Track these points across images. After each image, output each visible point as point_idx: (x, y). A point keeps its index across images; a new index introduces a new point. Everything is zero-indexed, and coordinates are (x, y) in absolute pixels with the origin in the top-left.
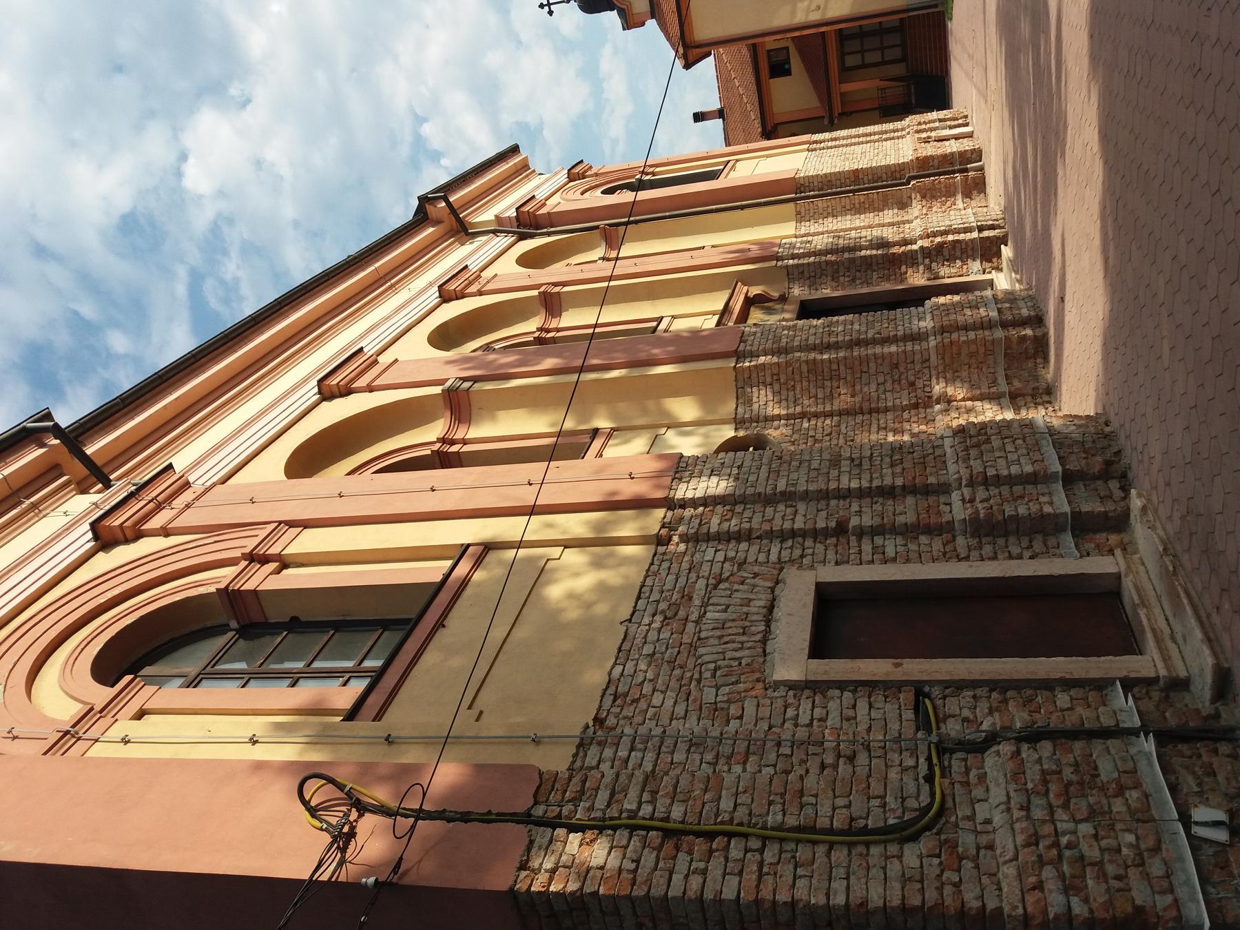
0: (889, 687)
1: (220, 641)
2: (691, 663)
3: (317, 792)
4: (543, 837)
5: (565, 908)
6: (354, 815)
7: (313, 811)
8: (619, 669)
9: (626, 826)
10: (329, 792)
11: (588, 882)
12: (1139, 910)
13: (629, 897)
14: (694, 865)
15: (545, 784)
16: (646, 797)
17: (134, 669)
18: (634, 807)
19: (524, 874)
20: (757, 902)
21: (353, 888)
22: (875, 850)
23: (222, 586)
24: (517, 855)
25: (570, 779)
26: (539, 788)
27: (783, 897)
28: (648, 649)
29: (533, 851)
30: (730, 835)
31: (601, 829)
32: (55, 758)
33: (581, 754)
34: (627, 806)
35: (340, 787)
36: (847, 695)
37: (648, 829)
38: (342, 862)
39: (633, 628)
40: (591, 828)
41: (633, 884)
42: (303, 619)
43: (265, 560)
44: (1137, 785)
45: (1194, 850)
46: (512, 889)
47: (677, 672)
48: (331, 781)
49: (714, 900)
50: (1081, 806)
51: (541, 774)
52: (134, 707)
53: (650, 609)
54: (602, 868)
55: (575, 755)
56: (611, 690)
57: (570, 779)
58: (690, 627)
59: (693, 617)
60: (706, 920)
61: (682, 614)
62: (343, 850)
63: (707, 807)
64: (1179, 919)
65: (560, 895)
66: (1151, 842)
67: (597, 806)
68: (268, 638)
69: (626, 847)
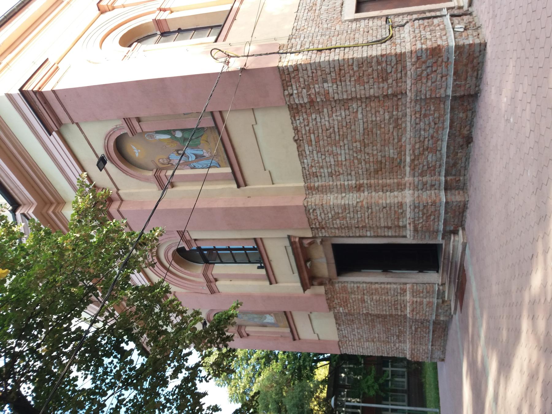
0: (378, 17)
1: (155, 38)
2: (319, 19)
3: (216, 54)
7: (216, 59)
8: (296, 24)
12: (439, 46)
13: (310, 64)
16: (311, 44)
20: (344, 59)
21: (234, 73)
22: (374, 46)
27: (350, 57)
28: (305, 18)
30: (335, 48)
31: (300, 53)
34: (306, 47)
36: (367, 21)
38: (228, 67)
39: (298, 14)
42: (182, 29)
43: (165, 10)
44: (443, 24)
45: (454, 34)
47: (315, 22)
48: (220, 50)
50: (428, 29)
53: (303, 9)
56: (295, 28)
58: (317, 11)
59: (318, 8)
61: (314, 8)
64: (448, 46)
66: (444, 33)
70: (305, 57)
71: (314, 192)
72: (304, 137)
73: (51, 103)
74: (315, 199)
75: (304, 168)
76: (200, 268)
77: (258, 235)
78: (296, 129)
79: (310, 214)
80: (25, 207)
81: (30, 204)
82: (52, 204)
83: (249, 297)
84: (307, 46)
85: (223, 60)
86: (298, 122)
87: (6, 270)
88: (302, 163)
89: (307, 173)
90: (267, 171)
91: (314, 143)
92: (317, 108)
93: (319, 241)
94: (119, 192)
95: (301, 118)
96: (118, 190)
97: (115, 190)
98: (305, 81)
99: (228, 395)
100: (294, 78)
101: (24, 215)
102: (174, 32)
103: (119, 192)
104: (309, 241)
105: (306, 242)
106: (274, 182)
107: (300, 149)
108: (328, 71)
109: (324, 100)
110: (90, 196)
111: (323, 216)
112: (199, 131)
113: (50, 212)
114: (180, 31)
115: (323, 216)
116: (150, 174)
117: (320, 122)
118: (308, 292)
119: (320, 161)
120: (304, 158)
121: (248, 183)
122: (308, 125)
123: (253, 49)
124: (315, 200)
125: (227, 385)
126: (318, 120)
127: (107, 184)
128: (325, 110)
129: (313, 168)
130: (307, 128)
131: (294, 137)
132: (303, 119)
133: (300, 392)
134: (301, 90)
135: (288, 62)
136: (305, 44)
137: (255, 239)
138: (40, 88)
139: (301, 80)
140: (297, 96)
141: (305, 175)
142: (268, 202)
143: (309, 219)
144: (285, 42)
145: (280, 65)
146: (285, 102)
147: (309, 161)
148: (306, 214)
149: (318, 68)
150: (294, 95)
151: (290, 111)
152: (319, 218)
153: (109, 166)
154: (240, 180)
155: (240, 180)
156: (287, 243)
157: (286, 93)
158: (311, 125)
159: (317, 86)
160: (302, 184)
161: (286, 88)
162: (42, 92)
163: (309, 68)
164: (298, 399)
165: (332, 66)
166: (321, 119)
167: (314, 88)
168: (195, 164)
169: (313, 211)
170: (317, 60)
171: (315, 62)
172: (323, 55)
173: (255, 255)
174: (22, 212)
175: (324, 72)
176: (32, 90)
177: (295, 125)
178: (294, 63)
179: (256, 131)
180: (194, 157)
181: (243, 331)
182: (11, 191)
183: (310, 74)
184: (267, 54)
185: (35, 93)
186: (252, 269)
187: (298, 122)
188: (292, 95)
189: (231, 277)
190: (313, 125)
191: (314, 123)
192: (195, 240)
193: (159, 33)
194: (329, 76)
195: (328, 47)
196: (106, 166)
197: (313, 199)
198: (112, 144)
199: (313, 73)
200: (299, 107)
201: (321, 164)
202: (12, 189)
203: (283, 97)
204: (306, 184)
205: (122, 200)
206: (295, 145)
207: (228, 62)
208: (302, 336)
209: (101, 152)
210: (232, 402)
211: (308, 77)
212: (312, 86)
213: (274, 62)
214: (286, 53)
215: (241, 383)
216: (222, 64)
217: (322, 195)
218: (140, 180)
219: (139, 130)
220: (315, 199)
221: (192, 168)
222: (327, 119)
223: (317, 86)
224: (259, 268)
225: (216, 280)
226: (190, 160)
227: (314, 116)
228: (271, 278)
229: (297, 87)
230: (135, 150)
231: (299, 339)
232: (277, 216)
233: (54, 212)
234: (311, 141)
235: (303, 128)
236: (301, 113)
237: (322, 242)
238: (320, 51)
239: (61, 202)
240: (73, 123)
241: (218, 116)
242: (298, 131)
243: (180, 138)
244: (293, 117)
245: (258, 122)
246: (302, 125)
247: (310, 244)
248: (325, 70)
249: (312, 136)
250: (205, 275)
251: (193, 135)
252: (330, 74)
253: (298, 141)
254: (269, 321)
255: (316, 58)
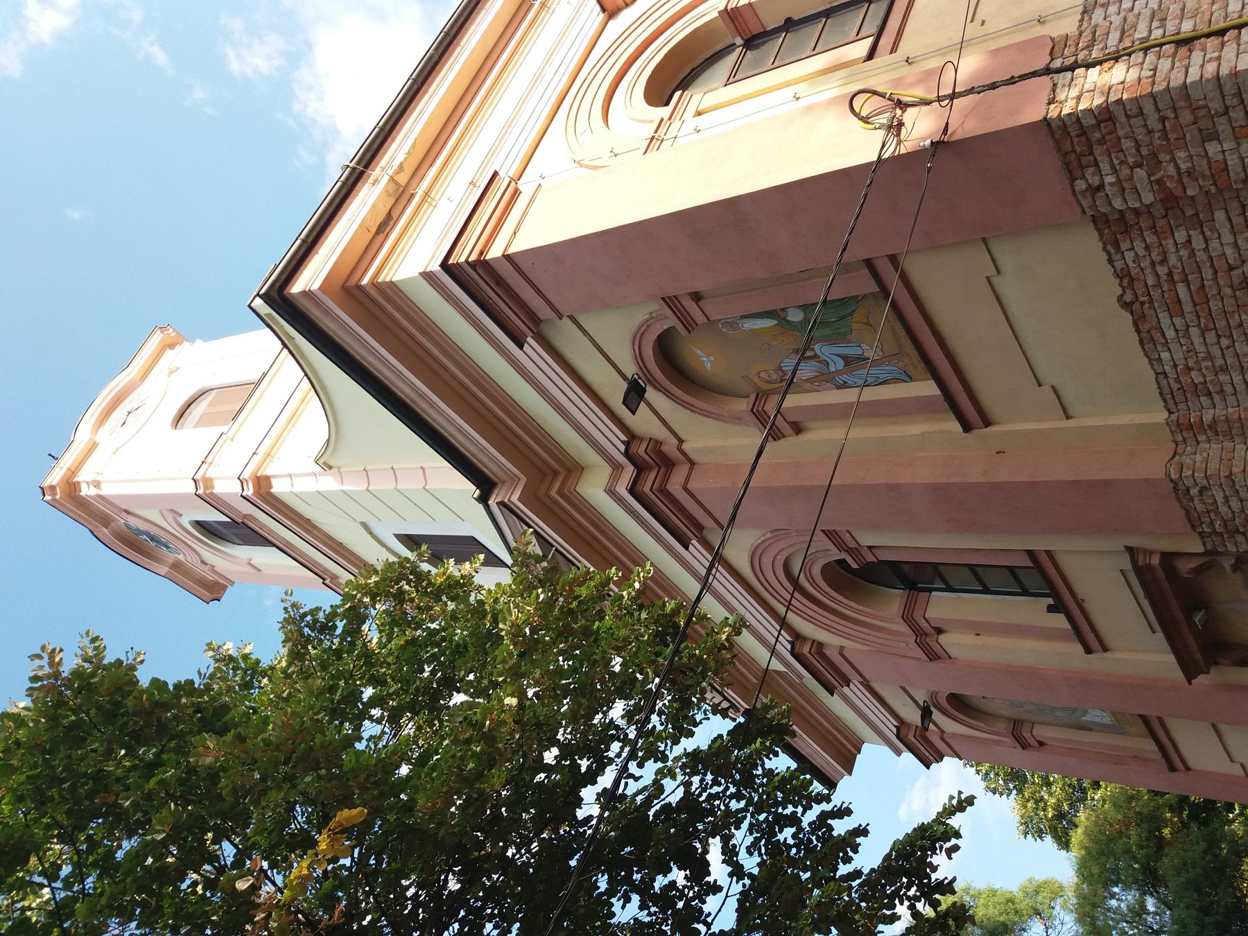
1: (731, 59)
3: (866, 105)
4: (1064, 78)
5: (1094, 122)
6: (899, 112)
7: (866, 120)
9: (1140, 50)
10: (876, 102)
11: (1112, 94)
13: (1152, 96)
14: (1208, 56)
15: (1055, 46)
16: (1155, 24)
17: (684, 84)
18: (1145, 34)
19: (1052, 106)
23: (722, 7)
24: (1045, 96)
25: (1080, 34)
26: (1053, 48)
29: (1058, 90)
31: (1117, 59)
32: (652, 154)
33: (1086, 18)
34: (1137, 36)
35: (882, 95)
37: (1161, 45)
38: (899, 143)
40: (1106, 61)
41: (1154, 83)
42: (796, 18)
46: (1045, 119)
48: (875, 93)
49: (1230, 74)
51: (1052, 40)
52: (691, 110)
54: (1123, 83)
55: (1081, 20)
57: (1080, 34)
60: (1223, 96)
62: (898, 135)
63: (1215, 15)
65: (1089, 111)
67: (1109, 44)
68: (770, 44)
69: (1142, 63)
70: (1133, 74)
71: (1201, 438)
72: (1155, 294)
73: (509, 281)
74: (1207, 457)
75: (1160, 375)
76: (893, 601)
77: (1039, 544)
78: (1123, 275)
79: (1192, 499)
80: (505, 488)
81: (514, 480)
82: (556, 474)
83: (1030, 675)
84: (1141, 32)
85: (884, 119)
86: (1129, 256)
87: (359, 809)
88: (1154, 361)
89: (1175, 386)
90: (1047, 388)
91: (1188, 307)
92: (1190, 212)
93: (1227, 563)
94: (684, 446)
95: (1139, 247)
96: (681, 441)
97: (675, 441)
98: (1138, 146)
99: (1018, 819)
100: (1101, 142)
101: (502, 504)
102: (777, 31)
103: (684, 446)
104: (1194, 563)
105: (1184, 567)
106: (1071, 413)
107: (1144, 327)
108: (1216, 106)
109: (1213, 189)
110: (538, 596)
111: (1235, 503)
112: (846, 306)
113: (553, 493)
114: (790, 25)
115: (1235, 503)
116: (743, 406)
117: (1206, 249)
118: (1201, 680)
119: (1216, 351)
120: (1159, 348)
121: (992, 417)
122: (1164, 261)
123: (970, 66)
124: (1207, 460)
125: (1015, 792)
126: (1198, 243)
127: (659, 432)
128: (1220, 216)
129: (1193, 373)
130: (1162, 270)
131: (1120, 298)
132: (1147, 248)
133: (1205, 852)
134: (1128, 171)
135: (1079, 98)
136: (1135, 27)
137: (1031, 554)
138: (481, 253)
139: (1127, 144)
140: (1115, 189)
141: (1166, 390)
142: (1057, 471)
143: (1188, 512)
144: (1067, 26)
145: (1053, 112)
146: (1079, 210)
147: (1179, 356)
148: (1179, 500)
149: (1182, 104)
150: (1107, 187)
151: (1098, 230)
152: (1223, 509)
153: (651, 394)
154: (967, 409)
155: (967, 409)
156: (1126, 564)
157: (1081, 185)
158: (1173, 260)
159: (1181, 154)
160: (1161, 416)
161: (1078, 173)
162: (486, 261)
163: (1148, 108)
164: (1199, 870)
165: (1229, 89)
166: (1206, 241)
167: (1173, 160)
168: (845, 377)
169: (1201, 492)
170: (1177, 80)
171: (1168, 89)
172: (1197, 57)
173: (1037, 578)
174: (499, 500)
175: (1203, 112)
176: (467, 261)
177: (1119, 265)
178: (1099, 101)
179: (999, 290)
180: (840, 364)
181: (1027, 735)
182: (474, 460)
183: (1153, 121)
184: (1011, 81)
185: (473, 265)
186: (1033, 611)
187: (1129, 256)
188: (1101, 187)
189: (979, 629)
190: (1180, 259)
191: (1184, 253)
192: (870, 548)
193: (739, 41)
194: (1223, 120)
195: (1214, 27)
196: (647, 395)
197: (1198, 458)
198: (649, 352)
199: (1163, 119)
200: (1130, 217)
201: (1219, 362)
202: (474, 456)
203: (1070, 198)
204: (1174, 417)
205: (692, 463)
206: (1126, 318)
207: (901, 124)
208: (1193, 762)
209: (631, 369)
210: (1029, 836)
211: (1150, 132)
212: (1164, 157)
213: (1031, 106)
214: (1072, 68)
215: (1051, 794)
216: (881, 134)
217: (1228, 445)
218: (723, 421)
219: (700, 319)
220: (1207, 457)
221: (839, 387)
222: (1227, 238)
223: (1181, 154)
224: (1051, 609)
225: (939, 631)
226: (832, 369)
227: (1181, 236)
228: (1088, 636)
229: (1113, 167)
230: (704, 358)
231: (1188, 769)
232: (1089, 503)
233: (560, 493)
234: (1179, 302)
235: (1148, 271)
236: (1135, 233)
237: (1236, 568)
238: (1186, 42)
239: (574, 469)
240: (560, 316)
241: (885, 269)
242: (1132, 280)
243: (800, 322)
244: (1112, 246)
245: (1002, 268)
246: (1145, 263)
247: (1199, 570)
248: (1206, 106)
249: (1181, 289)
250: (908, 618)
251: (832, 317)
252: (1226, 112)
253: (1136, 306)
254: (1097, 720)
255: (1172, 72)
